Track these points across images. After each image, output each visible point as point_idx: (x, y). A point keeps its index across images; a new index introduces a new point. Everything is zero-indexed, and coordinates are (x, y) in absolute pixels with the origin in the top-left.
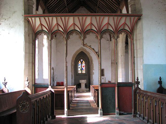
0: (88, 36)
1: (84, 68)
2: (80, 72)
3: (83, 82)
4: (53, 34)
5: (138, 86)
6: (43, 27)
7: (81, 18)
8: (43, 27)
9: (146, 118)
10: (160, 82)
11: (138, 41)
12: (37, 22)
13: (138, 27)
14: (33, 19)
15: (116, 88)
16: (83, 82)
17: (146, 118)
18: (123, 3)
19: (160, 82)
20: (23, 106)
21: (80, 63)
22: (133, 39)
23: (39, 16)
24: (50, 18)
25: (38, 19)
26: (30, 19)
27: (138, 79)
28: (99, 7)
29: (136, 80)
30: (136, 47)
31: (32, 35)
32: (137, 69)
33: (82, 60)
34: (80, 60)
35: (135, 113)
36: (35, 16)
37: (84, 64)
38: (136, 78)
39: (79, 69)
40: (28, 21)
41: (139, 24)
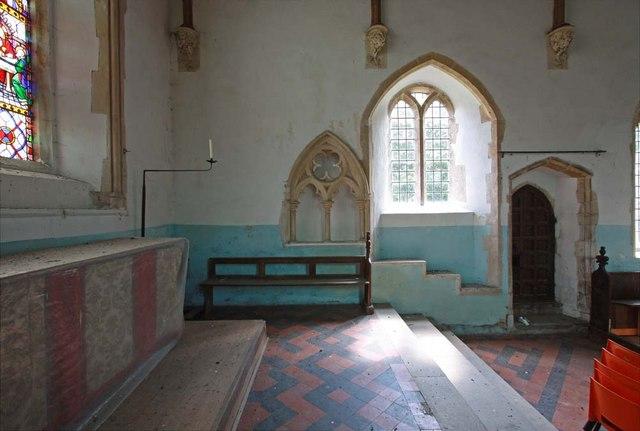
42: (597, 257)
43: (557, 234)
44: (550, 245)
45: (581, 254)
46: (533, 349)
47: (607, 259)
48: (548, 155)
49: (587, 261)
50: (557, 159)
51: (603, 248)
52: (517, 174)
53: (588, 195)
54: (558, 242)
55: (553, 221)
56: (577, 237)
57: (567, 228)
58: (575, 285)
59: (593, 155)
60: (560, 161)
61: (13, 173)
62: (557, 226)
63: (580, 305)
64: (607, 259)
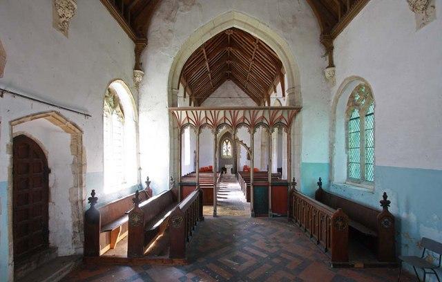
0: (239, 130)
1: (230, 150)
2: (225, 154)
3: (229, 167)
4: (199, 127)
5: (294, 187)
6: (190, 121)
7: (232, 111)
8: (190, 121)
9: (304, 225)
10: (320, 184)
11: (296, 136)
12: (183, 116)
13: (297, 120)
14: (179, 112)
15: (270, 187)
16: (229, 167)
17: (304, 225)
18: (278, 78)
19: (320, 184)
20: (177, 221)
21: (225, 143)
22: (290, 134)
23: (186, 109)
24: (198, 112)
25: (184, 112)
26: (175, 112)
27: (294, 180)
28: (251, 72)
29: (292, 181)
30: (294, 143)
31: (177, 131)
32: (294, 168)
33: (227, 141)
34: (225, 140)
35: (291, 216)
36: (181, 109)
37: (229, 145)
38: (292, 179)
39: (224, 151)
40: (173, 113)
41: (298, 116)
42: (381, 202)
43: (51, 184)
44: (44, 195)
45: (75, 199)
46: (365, 266)
47: (389, 202)
48: (51, 108)
49: (79, 204)
50: (58, 114)
51: (93, 191)
52: (20, 121)
53: (80, 149)
54: (52, 191)
55: (48, 171)
56: (71, 184)
57: (59, 177)
58: (69, 226)
59: (83, 116)
60: (62, 116)
61: (218, 162)
62: (51, 177)
63: (75, 243)
64: (389, 202)
